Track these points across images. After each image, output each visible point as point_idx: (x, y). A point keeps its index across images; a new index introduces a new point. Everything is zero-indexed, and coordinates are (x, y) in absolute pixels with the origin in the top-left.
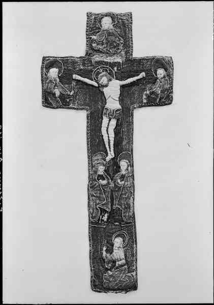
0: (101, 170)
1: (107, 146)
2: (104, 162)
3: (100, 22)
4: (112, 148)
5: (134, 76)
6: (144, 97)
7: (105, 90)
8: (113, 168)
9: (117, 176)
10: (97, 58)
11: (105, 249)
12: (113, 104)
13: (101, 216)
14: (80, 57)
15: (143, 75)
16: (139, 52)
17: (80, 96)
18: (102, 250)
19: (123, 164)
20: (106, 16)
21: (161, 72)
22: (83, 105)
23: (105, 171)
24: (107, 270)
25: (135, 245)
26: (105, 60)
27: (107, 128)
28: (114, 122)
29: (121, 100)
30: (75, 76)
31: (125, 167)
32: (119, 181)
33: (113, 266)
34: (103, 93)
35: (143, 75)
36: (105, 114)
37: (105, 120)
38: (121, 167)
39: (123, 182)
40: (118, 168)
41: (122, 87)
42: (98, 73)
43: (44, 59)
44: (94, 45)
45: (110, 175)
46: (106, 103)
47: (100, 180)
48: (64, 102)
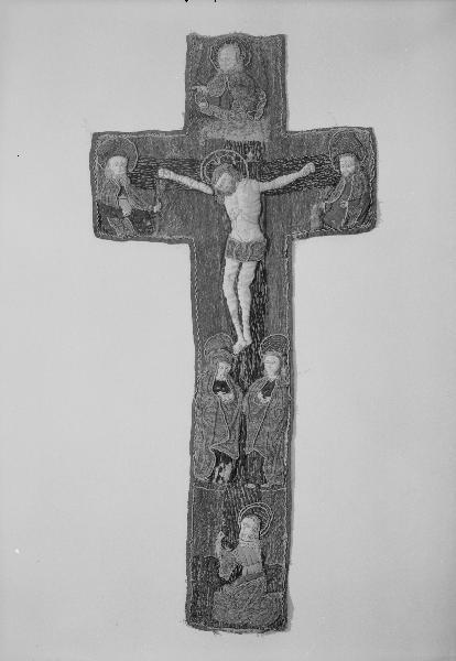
0: (222, 371)
1: (235, 321)
2: (228, 355)
3: (215, 57)
4: (246, 326)
5: (289, 171)
6: (314, 216)
7: (229, 203)
8: (247, 370)
9: (256, 388)
10: (209, 132)
11: (220, 536)
12: (244, 230)
13: (217, 469)
14: (173, 133)
15: (309, 168)
16: (302, 118)
17: (173, 217)
18: (214, 535)
19: (271, 362)
20: (228, 43)
21: (347, 165)
22: (180, 232)
23: (231, 374)
24: (223, 582)
25: (286, 535)
26: (228, 138)
27: (236, 284)
28: (248, 270)
29: (264, 221)
30: (163, 173)
31: (275, 367)
32: (260, 395)
33: (238, 574)
34: (223, 210)
35: (309, 168)
36: (230, 254)
37: (230, 265)
38: (266, 366)
39: (268, 399)
40: (257, 372)
41: (265, 195)
42: (211, 167)
43: (96, 136)
44: (202, 105)
45: (241, 384)
46: (230, 229)
47: (220, 393)
48: (143, 226)
